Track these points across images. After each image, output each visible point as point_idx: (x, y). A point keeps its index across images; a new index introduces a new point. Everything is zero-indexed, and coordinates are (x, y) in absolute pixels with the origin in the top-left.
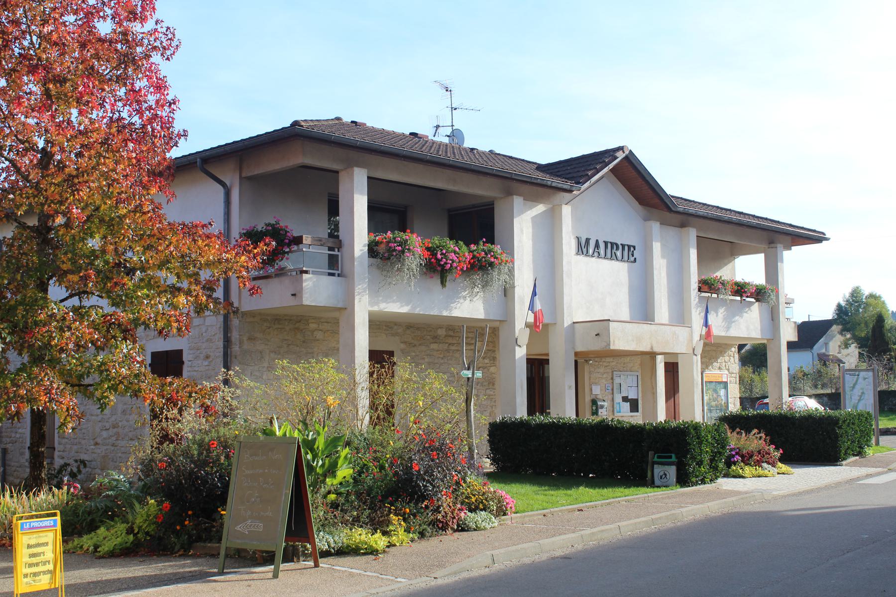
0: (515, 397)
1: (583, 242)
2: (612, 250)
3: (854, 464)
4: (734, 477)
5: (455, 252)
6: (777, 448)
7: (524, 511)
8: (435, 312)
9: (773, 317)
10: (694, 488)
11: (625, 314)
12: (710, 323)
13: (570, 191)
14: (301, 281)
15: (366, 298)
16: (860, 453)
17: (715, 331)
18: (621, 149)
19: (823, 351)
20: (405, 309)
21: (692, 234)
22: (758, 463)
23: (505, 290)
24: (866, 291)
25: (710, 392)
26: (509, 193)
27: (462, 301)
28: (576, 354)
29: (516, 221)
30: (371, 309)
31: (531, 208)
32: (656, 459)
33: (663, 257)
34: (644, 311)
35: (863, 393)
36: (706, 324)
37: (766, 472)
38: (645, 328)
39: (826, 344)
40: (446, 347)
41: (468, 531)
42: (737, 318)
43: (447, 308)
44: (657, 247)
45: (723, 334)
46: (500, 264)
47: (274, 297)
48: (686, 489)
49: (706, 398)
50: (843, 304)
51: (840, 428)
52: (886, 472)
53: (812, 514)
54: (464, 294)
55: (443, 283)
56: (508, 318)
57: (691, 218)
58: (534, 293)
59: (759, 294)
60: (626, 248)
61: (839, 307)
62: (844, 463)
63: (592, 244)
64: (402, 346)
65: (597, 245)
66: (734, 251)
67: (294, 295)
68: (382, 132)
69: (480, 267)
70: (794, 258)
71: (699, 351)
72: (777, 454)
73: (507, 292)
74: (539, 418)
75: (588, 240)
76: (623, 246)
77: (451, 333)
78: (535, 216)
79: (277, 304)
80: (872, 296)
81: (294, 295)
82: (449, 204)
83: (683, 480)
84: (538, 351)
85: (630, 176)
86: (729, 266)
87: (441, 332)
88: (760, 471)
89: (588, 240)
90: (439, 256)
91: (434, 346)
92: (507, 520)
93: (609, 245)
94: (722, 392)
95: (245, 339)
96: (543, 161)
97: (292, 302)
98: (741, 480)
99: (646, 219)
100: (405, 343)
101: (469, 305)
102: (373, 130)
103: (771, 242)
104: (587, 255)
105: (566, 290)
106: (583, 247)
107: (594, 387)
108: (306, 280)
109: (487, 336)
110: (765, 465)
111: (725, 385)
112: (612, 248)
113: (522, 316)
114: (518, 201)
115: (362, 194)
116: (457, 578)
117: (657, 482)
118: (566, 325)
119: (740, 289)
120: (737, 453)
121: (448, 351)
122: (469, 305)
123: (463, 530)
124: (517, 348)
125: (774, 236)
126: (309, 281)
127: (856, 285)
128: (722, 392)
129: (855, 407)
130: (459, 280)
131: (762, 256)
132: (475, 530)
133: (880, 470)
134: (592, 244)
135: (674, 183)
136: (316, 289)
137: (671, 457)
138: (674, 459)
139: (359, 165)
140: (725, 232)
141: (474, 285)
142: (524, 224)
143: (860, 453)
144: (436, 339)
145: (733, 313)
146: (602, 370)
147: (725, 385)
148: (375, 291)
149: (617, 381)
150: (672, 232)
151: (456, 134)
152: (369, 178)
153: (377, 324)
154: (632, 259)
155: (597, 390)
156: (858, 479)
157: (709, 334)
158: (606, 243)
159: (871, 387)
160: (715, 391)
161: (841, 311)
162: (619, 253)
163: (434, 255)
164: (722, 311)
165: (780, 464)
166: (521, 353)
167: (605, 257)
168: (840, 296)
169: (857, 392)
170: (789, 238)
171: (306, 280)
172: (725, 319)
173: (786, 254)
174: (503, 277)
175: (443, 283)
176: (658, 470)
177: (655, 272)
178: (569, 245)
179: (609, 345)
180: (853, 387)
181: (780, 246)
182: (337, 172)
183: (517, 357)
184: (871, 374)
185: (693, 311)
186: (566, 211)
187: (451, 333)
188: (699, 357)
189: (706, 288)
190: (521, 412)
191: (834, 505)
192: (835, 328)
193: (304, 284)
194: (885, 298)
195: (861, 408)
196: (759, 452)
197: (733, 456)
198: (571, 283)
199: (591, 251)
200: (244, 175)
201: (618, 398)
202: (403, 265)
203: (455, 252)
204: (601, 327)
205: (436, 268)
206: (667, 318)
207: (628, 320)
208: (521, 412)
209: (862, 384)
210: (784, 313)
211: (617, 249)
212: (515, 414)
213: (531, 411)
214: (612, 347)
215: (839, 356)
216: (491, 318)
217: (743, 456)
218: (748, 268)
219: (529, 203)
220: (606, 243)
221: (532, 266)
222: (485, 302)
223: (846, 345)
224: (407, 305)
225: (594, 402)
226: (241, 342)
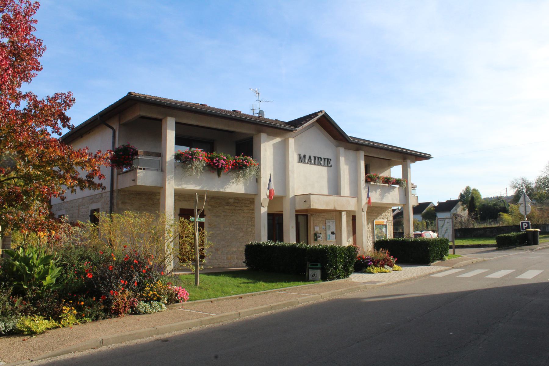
0: (260, 232)
1: (302, 156)
2: (318, 161)
3: (437, 265)
4: (369, 273)
5: (224, 160)
6: (394, 258)
7: (196, 300)
8: (215, 190)
9: (405, 194)
10: (332, 281)
11: (326, 192)
12: (370, 196)
13: (292, 131)
14: (136, 173)
15: (173, 182)
16: (442, 259)
17: (373, 200)
18: (321, 111)
19: (455, 212)
20: (198, 188)
21: (362, 154)
22: (382, 266)
23: (257, 179)
24: (472, 188)
25: (378, 229)
26: (260, 131)
27: (231, 184)
28: (297, 211)
29: (263, 146)
30: (177, 187)
31: (272, 139)
32: (310, 266)
33: (346, 164)
34: (335, 189)
35: (447, 229)
36: (368, 197)
37: (386, 270)
38: (336, 198)
39: (456, 210)
40: (234, 208)
41: (139, 314)
42: (387, 194)
43: (222, 187)
44: (342, 160)
45: (379, 202)
46: (251, 166)
47: (124, 182)
48: (326, 282)
49: (375, 232)
50: (463, 193)
51: (430, 247)
52: (450, 269)
53: (382, 301)
54: (233, 181)
55: (219, 175)
56: (258, 194)
57: (362, 147)
58: (270, 181)
59: (398, 182)
60: (326, 160)
61: (461, 194)
62: (432, 264)
63: (307, 158)
64: (210, 207)
65: (310, 158)
66: (390, 163)
67: (134, 180)
68: (215, 108)
69: (239, 168)
70: (415, 167)
71: (365, 209)
72: (395, 261)
73: (258, 180)
74: (278, 243)
75: (305, 156)
76: (325, 159)
77: (237, 201)
78: (275, 144)
79: (128, 186)
80: (474, 190)
81: (134, 180)
82: (226, 138)
83: (325, 278)
84: (275, 210)
85: (325, 123)
86: (388, 171)
87: (231, 201)
88: (383, 269)
89: (305, 156)
90: (215, 161)
91: (226, 207)
92: (178, 306)
93: (317, 159)
94: (384, 229)
95: (120, 203)
96: (287, 121)
97: (132, 184)
98: (370, 275)
99: (337, 146)
100: (211, 206)
101: (236, 187)
102: (210, 108)
103: (405, 159)
104: (304, 163)
105: (291, 179)
106: (302, 159)
107: (316, 227)
108: (139, 173)
109: (247, 202)
110: (386, 266)
111: (386, 226)
112: (318, 160)
113: (264, 194)
114: (263, 136)
115: (172, 130)
116: (122, 345)
117: (310, 278)
118: (291, 196)
119: (387, 181)
120: (371, 261)
121: (235, 210)
122: (236, 187)
123: (136, 314)
124: (262, 208)
125: (407, 157)
126: (140, 173)
127: (468, 185)
128: (384, 229)
129: (443, 236)
130: (230, 174)
131: (401, 166)
132: (144, 314)
133: (448, 267)
134: (307, 158)
135: (350, 130)
136: (144, 177)
137: (317, 265)
138: (319, 265)
139: (172, 116)
140: (379, 157)
141: (238, 177)
142: (267, 148)
143: (442, 259)
144: (228, 204)
145: (385, 191)
146: (320, 219)
147: (386, 226)
148: (178, 178)
149: (328, 224)
150: (351, 153)
151: (261, 113)
152: (176, 123)
153: (179, 196)
154: (330, 165)
155: (317, 229)
156: (433, 273)
157: (369, 202)
158: (315, 157)
159: (451, 227)
160: (380, 229)
161: (462, 196)
162: (322, 162)
163: (212, 161)
164: (379, 191)
165: (395, 265)
166: (264, 210)
167: (315, 164)
168: (461, 190)
169: (444, 229)
170: (414, 157)
171: (139, 173)
172: (380, 195)
173: (412, 165)
174: (253, 173)
175: (219, 175)
176: (311, 272)
177: (342, 172)
178: (293, 157)
179: (310, 206)
180: (442, 227)
181: (409, 161)
182: (161, 120)
183: (262, 212)
184: (451, 220)
185: (362, 191)
186: (291, 141)
187: (237, 201)
188: (366, 213)
189: (369, 180)
190: (264, 239)
191: (395, 294)
192: (460, 203)
193: (138, 175)
194: (480, 191)
195: (446, 237)
196: (384, 260)
197: (369, 262)
198: (295, 177)
199: (306, 161)
200: (121, 123)
201: (329, 233)
202: (192, 165)
203: (224, 160)
204: (306, 197)
205: (214, 167)
206: (349, 192)
207: (326, 193)
208: (264, 239)
209: (446, 225)
210: (411, 192)
211: (321, 160)
212: (260, 240)
213: (270, 237)
214: (312, 207)
215: (462, 214)
216: (249, 193)
217: (374, 262)
218: (396, 172)
219: (271, 137)
220: (315, 157)
221: (272, 167)
222: (245, 185)
223: (464, 210)
224: (199, 186)
225: (315, 234)
226: (117, 204)
